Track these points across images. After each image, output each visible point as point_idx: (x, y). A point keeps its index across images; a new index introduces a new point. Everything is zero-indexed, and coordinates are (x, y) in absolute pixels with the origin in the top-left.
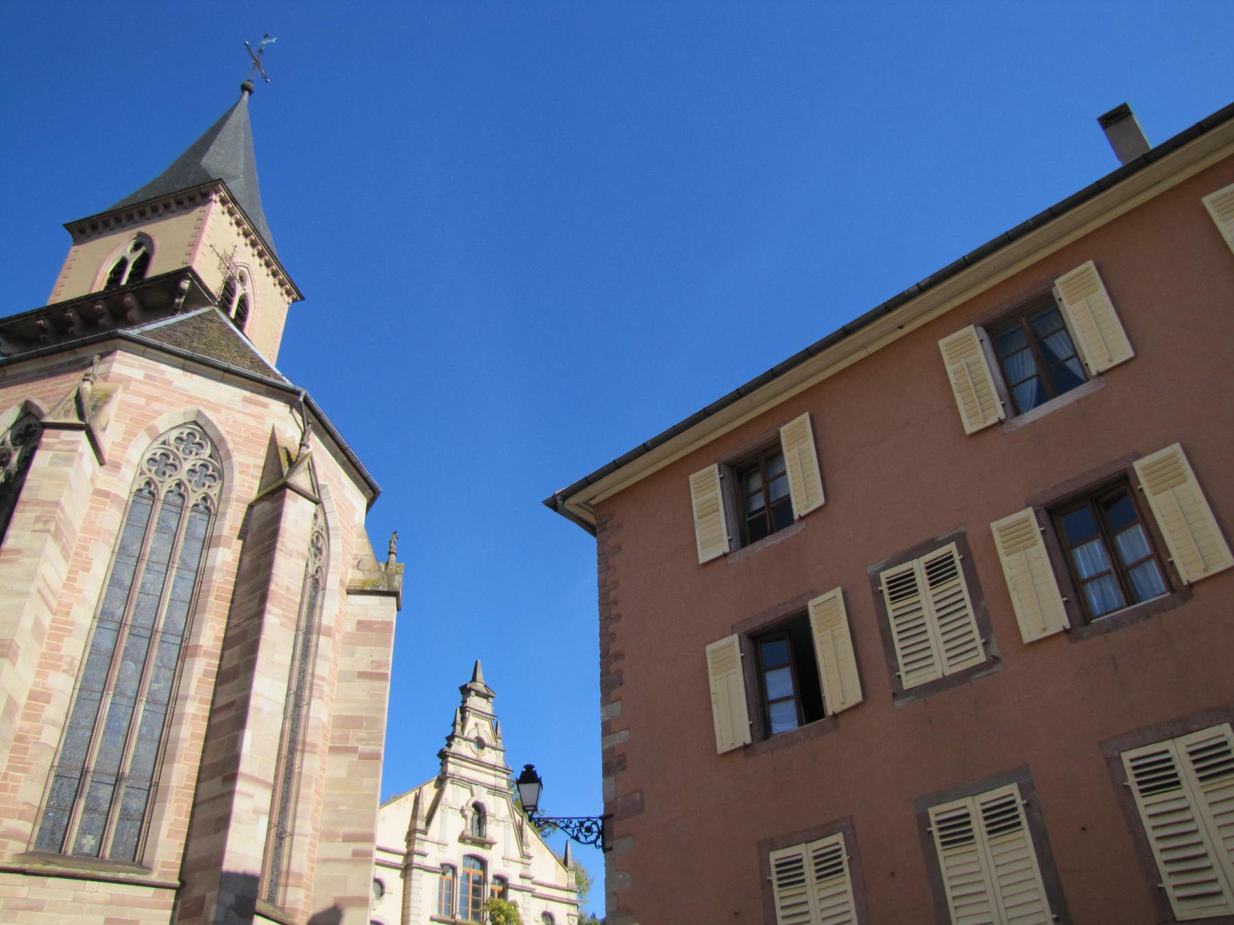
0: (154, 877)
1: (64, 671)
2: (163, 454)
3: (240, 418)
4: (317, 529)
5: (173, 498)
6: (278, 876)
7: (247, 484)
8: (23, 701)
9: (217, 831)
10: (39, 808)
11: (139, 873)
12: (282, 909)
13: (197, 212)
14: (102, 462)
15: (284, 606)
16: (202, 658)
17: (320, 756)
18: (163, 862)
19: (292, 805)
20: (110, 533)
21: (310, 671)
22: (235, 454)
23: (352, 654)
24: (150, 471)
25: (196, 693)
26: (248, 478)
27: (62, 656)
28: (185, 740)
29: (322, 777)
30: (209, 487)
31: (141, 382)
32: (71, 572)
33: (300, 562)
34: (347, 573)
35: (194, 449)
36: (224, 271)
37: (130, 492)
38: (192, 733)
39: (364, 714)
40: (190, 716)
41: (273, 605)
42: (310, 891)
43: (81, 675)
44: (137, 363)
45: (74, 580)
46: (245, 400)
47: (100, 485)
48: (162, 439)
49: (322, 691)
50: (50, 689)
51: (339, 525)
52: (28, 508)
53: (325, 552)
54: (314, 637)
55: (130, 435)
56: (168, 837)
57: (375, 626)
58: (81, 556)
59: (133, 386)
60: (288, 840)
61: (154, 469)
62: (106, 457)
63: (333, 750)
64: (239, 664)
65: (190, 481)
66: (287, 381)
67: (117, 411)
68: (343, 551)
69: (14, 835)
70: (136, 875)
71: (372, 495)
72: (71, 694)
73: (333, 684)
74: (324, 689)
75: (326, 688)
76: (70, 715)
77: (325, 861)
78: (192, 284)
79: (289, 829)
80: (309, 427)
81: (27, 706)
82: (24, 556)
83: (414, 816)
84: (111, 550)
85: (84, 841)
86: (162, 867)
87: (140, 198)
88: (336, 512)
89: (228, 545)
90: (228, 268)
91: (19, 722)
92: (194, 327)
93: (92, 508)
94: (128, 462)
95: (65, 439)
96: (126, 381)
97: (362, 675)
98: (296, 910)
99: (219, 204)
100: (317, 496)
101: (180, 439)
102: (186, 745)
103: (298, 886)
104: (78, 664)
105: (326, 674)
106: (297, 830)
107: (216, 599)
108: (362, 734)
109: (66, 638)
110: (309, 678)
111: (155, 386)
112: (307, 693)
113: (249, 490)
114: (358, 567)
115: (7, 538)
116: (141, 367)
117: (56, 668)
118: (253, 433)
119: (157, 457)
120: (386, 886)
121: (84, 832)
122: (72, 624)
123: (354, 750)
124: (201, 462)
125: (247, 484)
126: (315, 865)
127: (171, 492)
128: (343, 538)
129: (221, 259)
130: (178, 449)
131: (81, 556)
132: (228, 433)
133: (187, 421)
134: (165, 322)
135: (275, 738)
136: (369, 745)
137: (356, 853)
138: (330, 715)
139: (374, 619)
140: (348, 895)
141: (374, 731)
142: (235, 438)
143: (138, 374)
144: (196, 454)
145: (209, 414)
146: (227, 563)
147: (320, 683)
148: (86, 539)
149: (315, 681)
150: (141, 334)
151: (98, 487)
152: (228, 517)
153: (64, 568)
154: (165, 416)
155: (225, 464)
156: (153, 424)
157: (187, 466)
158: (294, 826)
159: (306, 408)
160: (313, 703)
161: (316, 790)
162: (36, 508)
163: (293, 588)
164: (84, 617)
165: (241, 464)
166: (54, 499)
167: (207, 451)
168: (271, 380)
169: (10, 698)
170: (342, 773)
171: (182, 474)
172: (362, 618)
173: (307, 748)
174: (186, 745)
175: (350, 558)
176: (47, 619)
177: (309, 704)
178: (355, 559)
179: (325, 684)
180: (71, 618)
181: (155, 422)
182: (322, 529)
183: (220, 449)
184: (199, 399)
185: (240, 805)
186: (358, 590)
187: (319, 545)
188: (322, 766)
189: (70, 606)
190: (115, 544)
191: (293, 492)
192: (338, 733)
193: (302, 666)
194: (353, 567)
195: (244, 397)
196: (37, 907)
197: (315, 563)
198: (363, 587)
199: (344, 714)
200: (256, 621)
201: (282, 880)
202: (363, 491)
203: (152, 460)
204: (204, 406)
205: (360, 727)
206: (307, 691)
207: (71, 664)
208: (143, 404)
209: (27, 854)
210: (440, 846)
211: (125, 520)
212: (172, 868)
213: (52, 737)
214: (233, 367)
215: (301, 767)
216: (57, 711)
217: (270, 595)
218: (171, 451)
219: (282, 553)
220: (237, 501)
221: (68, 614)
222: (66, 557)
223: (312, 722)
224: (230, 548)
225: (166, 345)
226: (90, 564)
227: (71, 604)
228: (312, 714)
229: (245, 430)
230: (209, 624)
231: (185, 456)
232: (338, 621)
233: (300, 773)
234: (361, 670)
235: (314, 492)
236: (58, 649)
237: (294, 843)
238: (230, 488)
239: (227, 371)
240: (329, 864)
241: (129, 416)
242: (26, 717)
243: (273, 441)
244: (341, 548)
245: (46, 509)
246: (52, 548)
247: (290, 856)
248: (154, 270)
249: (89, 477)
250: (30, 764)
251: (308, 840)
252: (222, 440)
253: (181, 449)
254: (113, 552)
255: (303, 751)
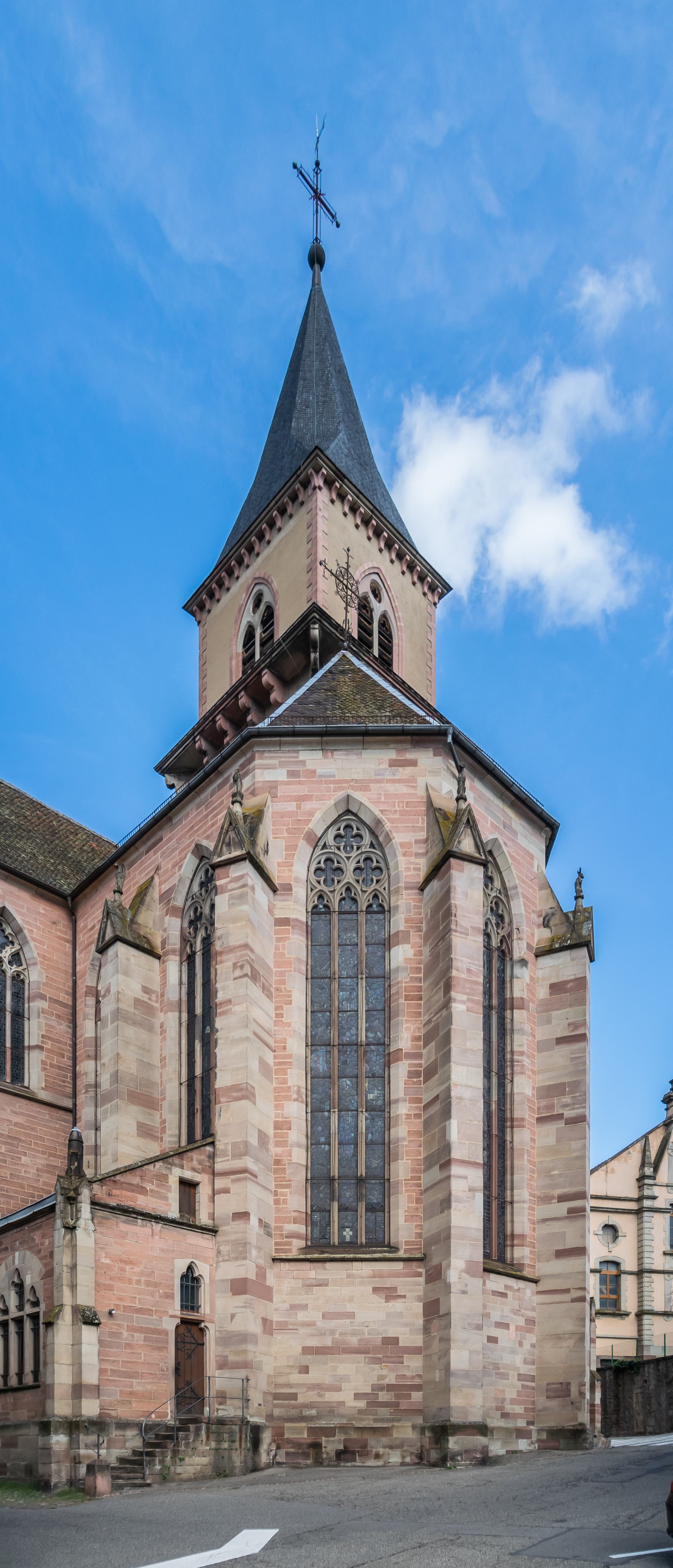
0: (401, 1254)
1: (295, 1100)
2: (327, 860)
3: (391, 788)
4: (494, 894)
5: (348, 906)
6: (505, 1239)
7: (412, 867)
8: (271, 1132)
9: (442, 1212)
10: (306, 1213)
11: (389, 1252)
12: (512, 1265)
13: (300, 517)
14: (274, 890)
15: (468, 991)
16: (404, 1061)
17: (528, 1128)
18: (405, 1242)
19: (508, 1177)
20: (299, 960)
21: (509, 1048)
22: (394, 834)
23: (549, 1021)
24: (319, 882)
25: (405, 1095)
26: (413, 859)
27: (290, 1087)
28: (404, 1139)
29: (533, 1148)
30: (378, 881)
31: (287, 783)
32: (277, 1008)
33: (476, 939)
34: (533, 935)
35: (354, 844)
36: (343, 593)
37: (307, 912)
38: (409, 1132)
39: (567, 1080)
40: (404, 1117)
41: (457, 992)
42: (534, 1247)
43: (309, 1100)
44: (275, 762)
45: (281, 1015)
46: (393, 764)
47: (280, 914)
48: (321, 843)
49: (523, 1066)
50: (289, 1118)
51: (517, 882)
52: (224, 957)
53: (507, 920)
54: (508, 1013)
55: (291, 848)
56: (405, 1222)
57: (568, 986)
58: (281, 991)
59: (281, 791)
60: (509, 1208)
61: (322, 879)
62: (276, 882)
63: (540, 1120)
64: (436, 1059)
65: (358, 881)
66: (431, 720)
67: (273, 826)
68: (526, 910)
69: (297, 1236)
70: (387, 1254)
71: (550, 833)
72: (305, 1118)
73: (534, 1056)
74: (525, 1063)
75: (526, 1061)
76: (309, 1136)
77: (544, 1220)
78: (322, 629)
79: (508, 1199)
80: (466, 771)
81: (276, 1135)
82: (234, 1005)
83: (643, 1165)
84: (305, 977)
85: (345, 1233)
86: (405, 1245)
87: (243, 527)
88: (512, 867)
89: (407, 941)
90: (347, 587)
91: (274, 1150)
92: (326, 690)
93: (278, 940)
94: (297, 880)
95: (234, 875)
96: (272, 787)
97: (560, 1041)
98: (523, 1264)
99: (325, 490)
100: (484, 857)
101: (338, 836)
102: (406, 1143)
103: (523, 1245)
104: (304, 1091)
105: (525, 1049)
106: (515, 1198)
107: (405, 1000)
108: (567, 1099)
109: (289, 1071)
110: (508, 1056)
111: (300, 783)
112: (509, 1071)
113: (416, 873)
114: (546, 924)
115: (216, 992)
116: (282, 765)
117: (288, 1098)
118: (407, 803)
119: (322, 865)
120: (619, 1230)
121: (342, 1228)
122: (290, 1056)
123: (560, 1116)
124: (364, 856)
125: (412, 867)
126: (536, 1226)
127: (343, 899)
128: (524, 896)
129: (337, 577)
130: (339, 849)
131: (281, 991)
132: (382, 811)
133: (340, 813)
134: (294, 696)
135: (479, 1122)
136: (574, 1109)
137: (571, 1211)
138: (533, 1088)
139: (566, 978)
140: (566, 1247)
141: (577, 1094)
142: (391, 816)
143: (280, 775)
144: (358, 848)
145: (358, 795)
146: (410, 959)
147: (520, 1058)
148: (282, 974)
149: (515, 1057)
150: (272, 723)
151: (277, 917)
152: (401, 909)
153: (270, 1007)
154: (318, 815)
155: (387, 850)
156: (309, 828)
157: (351, 866)
158: (512, 1196)
159: (458, 749)
160: (515, 1079)
161: (528, 1160)
162: (231, 955)
163: (473, 968)
164: (297, 1047)
165: (402, 845)
166: (242, 942)
167: (367, 839)
168: (415, 726)
169: (260, 1131)
170: (552, 1140)
171: (349, 877)
172: (554, 980)
173: (515, 1123)
174: (406, 1143)
175: (534, 916)
176: (269, 1058)
177: (512, 1081)
178: (539, 916)
179: (524, 1058)
180: (288, 1052)
181: (310, 826)
182: (500, 893)
183: (378, 834)
184: (346, 781)
185: (457, 1187)
186: (547, 951)
187: (500, 912)
188: (531, 1138)
189: (284, 1041)
190: (307, 970)
191: (457, 861)
192: (543, 1103)
193: (501, 1045)
194: (539, 926)
195: (390, 760)
196: (323, 1284)
197: (498, 933)
198: (551, 946)
199: (547, 1084)
200: (444, 1013)
201: (509, 1243)
202: (540, 829)
203: (318, 869)
204: (353, 788)
205: (563, 1094)
206: (508, 1069)
207: (298, 1092)
208: (295, 809)
209: (307, 1247)
210: (669, 1188)
211: (310, 943)
212: (416, 1245)
213: (300, 1156)
214: (371, 726)
215: (512, 1142)
216: (298, 1134)
217: (454, 982)
218: (334, 853)
219: (458, 934)
220: (406, 888)
221: (285, 1048)
222: (269, 996)
223: (516, 1098)
224: (409, 943)
225: (299, 726)
226: (290, 996)
227: (285, 1039)
228: (516, 1091)
229: (399, 802)
230: (404, 1026)
231: (347, 855)
232: (531, 990)
233: (512, 1148)
234: (559, 1036)
235: (480, 853)
236: (285, 1081)
237: (515, 1210)
238: (397, 876)
239: (366, 733)
240: (548, 1223)
241: (285, 828)
242: (277, 1144)
243: (430, 803)
244: (523, 908)
245: (238, 954)
246: (255, 991)
247: (512, 1221)
248: (281, 628)
249: (266, 908)
250: (290, 1181)
251: (526, 1206)
252: (379, 822)
253: (342, 848)
254: (307, 979)
255: (512, 1127)
